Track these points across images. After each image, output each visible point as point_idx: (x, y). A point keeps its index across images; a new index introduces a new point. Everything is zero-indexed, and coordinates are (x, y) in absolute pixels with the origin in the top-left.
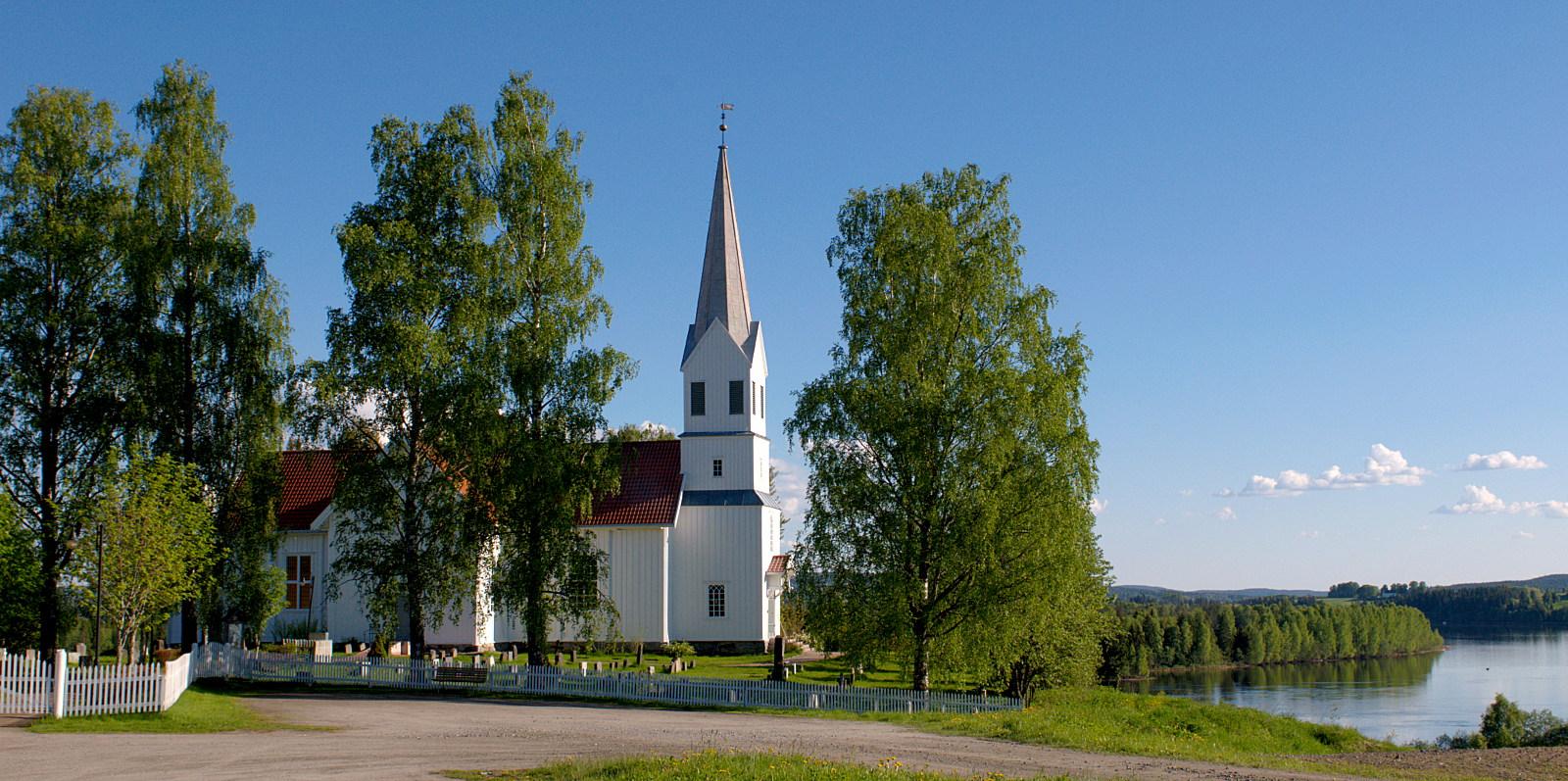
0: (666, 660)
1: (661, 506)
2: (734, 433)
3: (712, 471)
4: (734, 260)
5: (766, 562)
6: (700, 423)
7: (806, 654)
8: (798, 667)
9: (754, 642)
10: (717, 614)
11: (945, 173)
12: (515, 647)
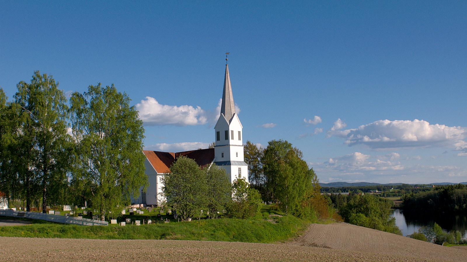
2: (225, 145)
6: (219, 143)
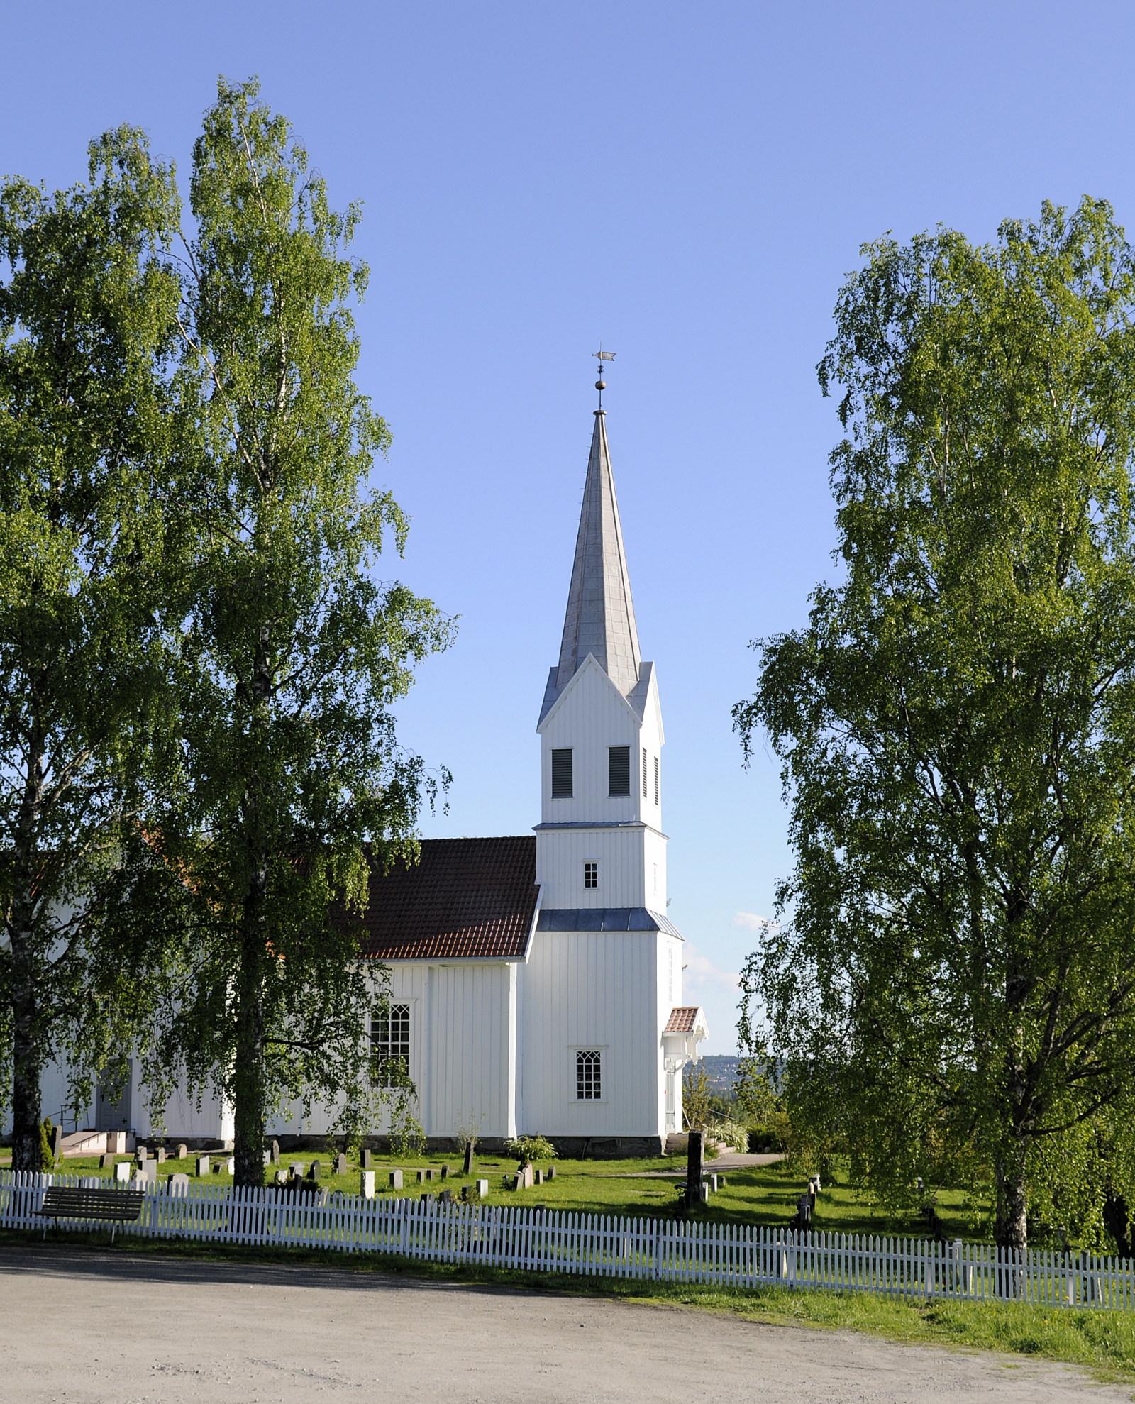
0: (508, 1167)
1: (506, 931)
2: (616, 825)
3: (583, 880)
4: (616, 571)
5: (663, 1018)
7: (724, 1158)
8: (720, 1179)
9: (645, 1139)
10: (589, 1095)
11: (1046, 209)
12: (275, 1143)
